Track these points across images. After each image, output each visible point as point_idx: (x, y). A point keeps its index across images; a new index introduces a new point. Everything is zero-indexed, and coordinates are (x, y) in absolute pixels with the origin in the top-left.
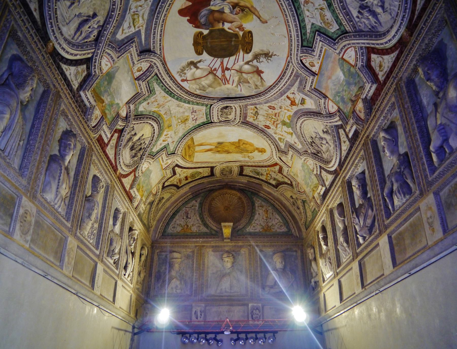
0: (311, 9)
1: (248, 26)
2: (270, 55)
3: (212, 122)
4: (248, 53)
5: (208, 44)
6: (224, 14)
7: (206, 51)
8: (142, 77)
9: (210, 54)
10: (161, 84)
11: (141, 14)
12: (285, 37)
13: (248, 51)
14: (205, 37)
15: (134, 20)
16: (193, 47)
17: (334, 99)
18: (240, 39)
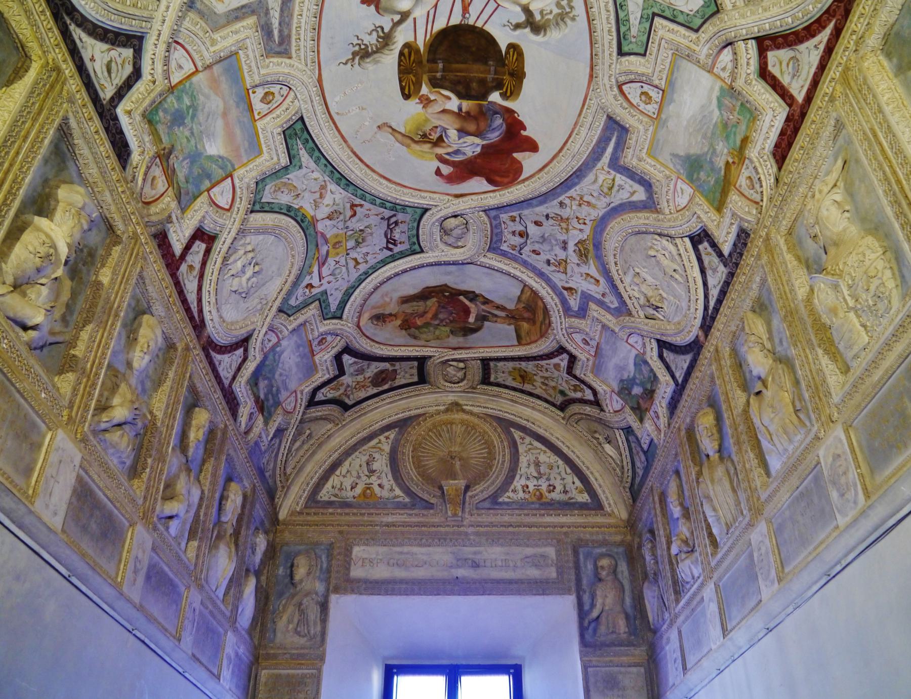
1: (413, 107)
2: (357, 58)
4: (407, 45)
5: (492, 69)
6: (457, 126)
7: (501, 51)
9: (490, 41)
10: (622, 15)
11: (596, 187)
12: (338, 114)
13: (406, 51)
14: (499, 86)
15: (610, 189)
16: (527, 69)
17: (191, 84)
18: (425, 78)
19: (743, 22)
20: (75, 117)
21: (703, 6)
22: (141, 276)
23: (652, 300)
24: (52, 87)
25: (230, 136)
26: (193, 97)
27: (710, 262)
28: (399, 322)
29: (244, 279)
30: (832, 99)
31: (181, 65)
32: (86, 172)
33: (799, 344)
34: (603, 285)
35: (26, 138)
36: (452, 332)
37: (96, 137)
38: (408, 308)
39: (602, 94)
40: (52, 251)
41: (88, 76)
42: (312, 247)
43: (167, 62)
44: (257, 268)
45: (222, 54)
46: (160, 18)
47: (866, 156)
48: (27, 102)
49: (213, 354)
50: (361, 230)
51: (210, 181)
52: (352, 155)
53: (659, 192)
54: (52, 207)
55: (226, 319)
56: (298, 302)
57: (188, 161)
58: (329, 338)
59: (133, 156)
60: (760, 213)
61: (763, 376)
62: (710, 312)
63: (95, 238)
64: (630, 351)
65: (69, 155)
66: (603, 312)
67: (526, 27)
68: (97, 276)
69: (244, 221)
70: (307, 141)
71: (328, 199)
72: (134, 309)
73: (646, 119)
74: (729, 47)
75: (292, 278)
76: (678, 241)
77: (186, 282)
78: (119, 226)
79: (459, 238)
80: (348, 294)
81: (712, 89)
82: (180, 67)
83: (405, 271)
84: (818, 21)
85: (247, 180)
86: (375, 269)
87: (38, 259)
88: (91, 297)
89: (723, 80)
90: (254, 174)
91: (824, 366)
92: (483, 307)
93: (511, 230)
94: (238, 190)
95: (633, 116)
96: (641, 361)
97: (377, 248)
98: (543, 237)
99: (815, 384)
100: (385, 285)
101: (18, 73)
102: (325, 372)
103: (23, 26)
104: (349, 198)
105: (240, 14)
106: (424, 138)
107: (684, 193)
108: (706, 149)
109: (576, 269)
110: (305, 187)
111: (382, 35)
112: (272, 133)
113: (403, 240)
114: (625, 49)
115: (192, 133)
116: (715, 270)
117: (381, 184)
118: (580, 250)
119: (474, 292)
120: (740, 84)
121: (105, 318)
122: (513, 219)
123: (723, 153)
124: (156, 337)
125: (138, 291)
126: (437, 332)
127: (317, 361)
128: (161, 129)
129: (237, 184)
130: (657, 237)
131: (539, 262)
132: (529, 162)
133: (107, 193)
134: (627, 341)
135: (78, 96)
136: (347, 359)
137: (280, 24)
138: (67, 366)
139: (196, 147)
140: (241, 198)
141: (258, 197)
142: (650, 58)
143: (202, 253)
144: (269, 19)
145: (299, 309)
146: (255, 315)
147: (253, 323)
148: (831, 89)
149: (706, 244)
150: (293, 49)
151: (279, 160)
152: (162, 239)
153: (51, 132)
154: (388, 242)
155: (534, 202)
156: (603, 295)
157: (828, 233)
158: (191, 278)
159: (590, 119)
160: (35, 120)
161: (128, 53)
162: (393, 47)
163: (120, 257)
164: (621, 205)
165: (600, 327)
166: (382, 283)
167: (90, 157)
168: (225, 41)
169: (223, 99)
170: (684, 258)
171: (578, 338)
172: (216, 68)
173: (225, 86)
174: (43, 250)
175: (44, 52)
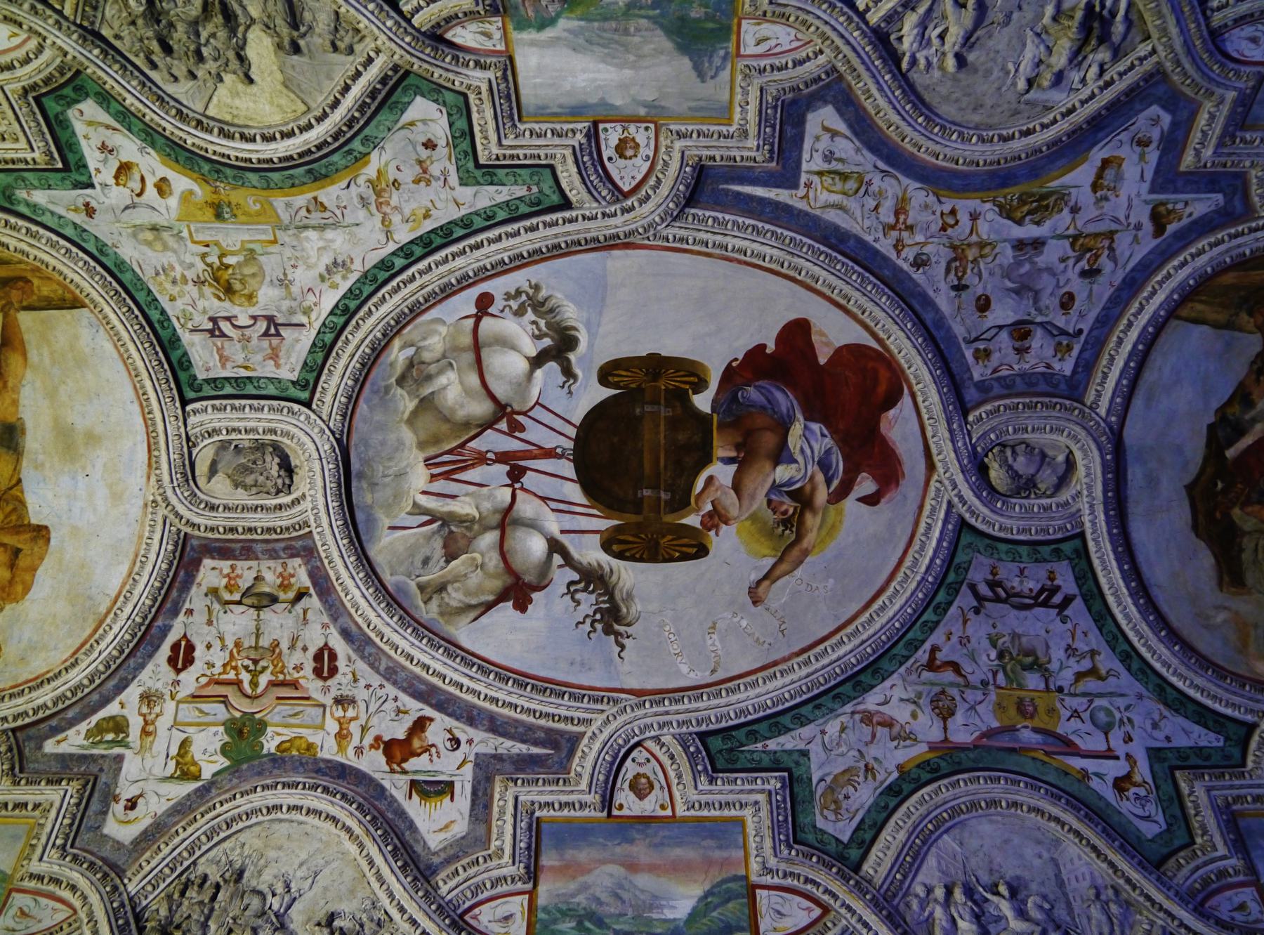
0: (851, 736)
1: (724, 542)
2: (616, 627)
3: (184, 402)
4: (606, 547)
5: (648, 408)
6: (768, 466)
7: (615, 396)
8: (591, 154)
9: (597, 414)
10: (502, 215)
11: (852, 204)
12: (713, 671)
13: (615, 547)
14: (680, 398)
15: (844, 177)
17: (545, 909)
18: (668, 518)
25: (678, 869)
42: (1011, 761)
50: (1001, 656)
56: (1160, 818)
67: (568, 361)
71: (901, 714)
80: (1179, 703)
81: (533, 43)
93: (1012, 357)
97: (1058, 626)
100: (1173, 619)
104: (909, 671)
105: (482, 801)
108: (643, 22)
109: (1089, 211)
111: (582, 585)
119: (1211, 428)
137: (524, 742)
144: (510, 757)
154: (1045, 604)
155: (928, 317)
156: (1143, 143)
162: (607, 569)
164: (873, 149)
169: (603, 862)
173: (583, 855)
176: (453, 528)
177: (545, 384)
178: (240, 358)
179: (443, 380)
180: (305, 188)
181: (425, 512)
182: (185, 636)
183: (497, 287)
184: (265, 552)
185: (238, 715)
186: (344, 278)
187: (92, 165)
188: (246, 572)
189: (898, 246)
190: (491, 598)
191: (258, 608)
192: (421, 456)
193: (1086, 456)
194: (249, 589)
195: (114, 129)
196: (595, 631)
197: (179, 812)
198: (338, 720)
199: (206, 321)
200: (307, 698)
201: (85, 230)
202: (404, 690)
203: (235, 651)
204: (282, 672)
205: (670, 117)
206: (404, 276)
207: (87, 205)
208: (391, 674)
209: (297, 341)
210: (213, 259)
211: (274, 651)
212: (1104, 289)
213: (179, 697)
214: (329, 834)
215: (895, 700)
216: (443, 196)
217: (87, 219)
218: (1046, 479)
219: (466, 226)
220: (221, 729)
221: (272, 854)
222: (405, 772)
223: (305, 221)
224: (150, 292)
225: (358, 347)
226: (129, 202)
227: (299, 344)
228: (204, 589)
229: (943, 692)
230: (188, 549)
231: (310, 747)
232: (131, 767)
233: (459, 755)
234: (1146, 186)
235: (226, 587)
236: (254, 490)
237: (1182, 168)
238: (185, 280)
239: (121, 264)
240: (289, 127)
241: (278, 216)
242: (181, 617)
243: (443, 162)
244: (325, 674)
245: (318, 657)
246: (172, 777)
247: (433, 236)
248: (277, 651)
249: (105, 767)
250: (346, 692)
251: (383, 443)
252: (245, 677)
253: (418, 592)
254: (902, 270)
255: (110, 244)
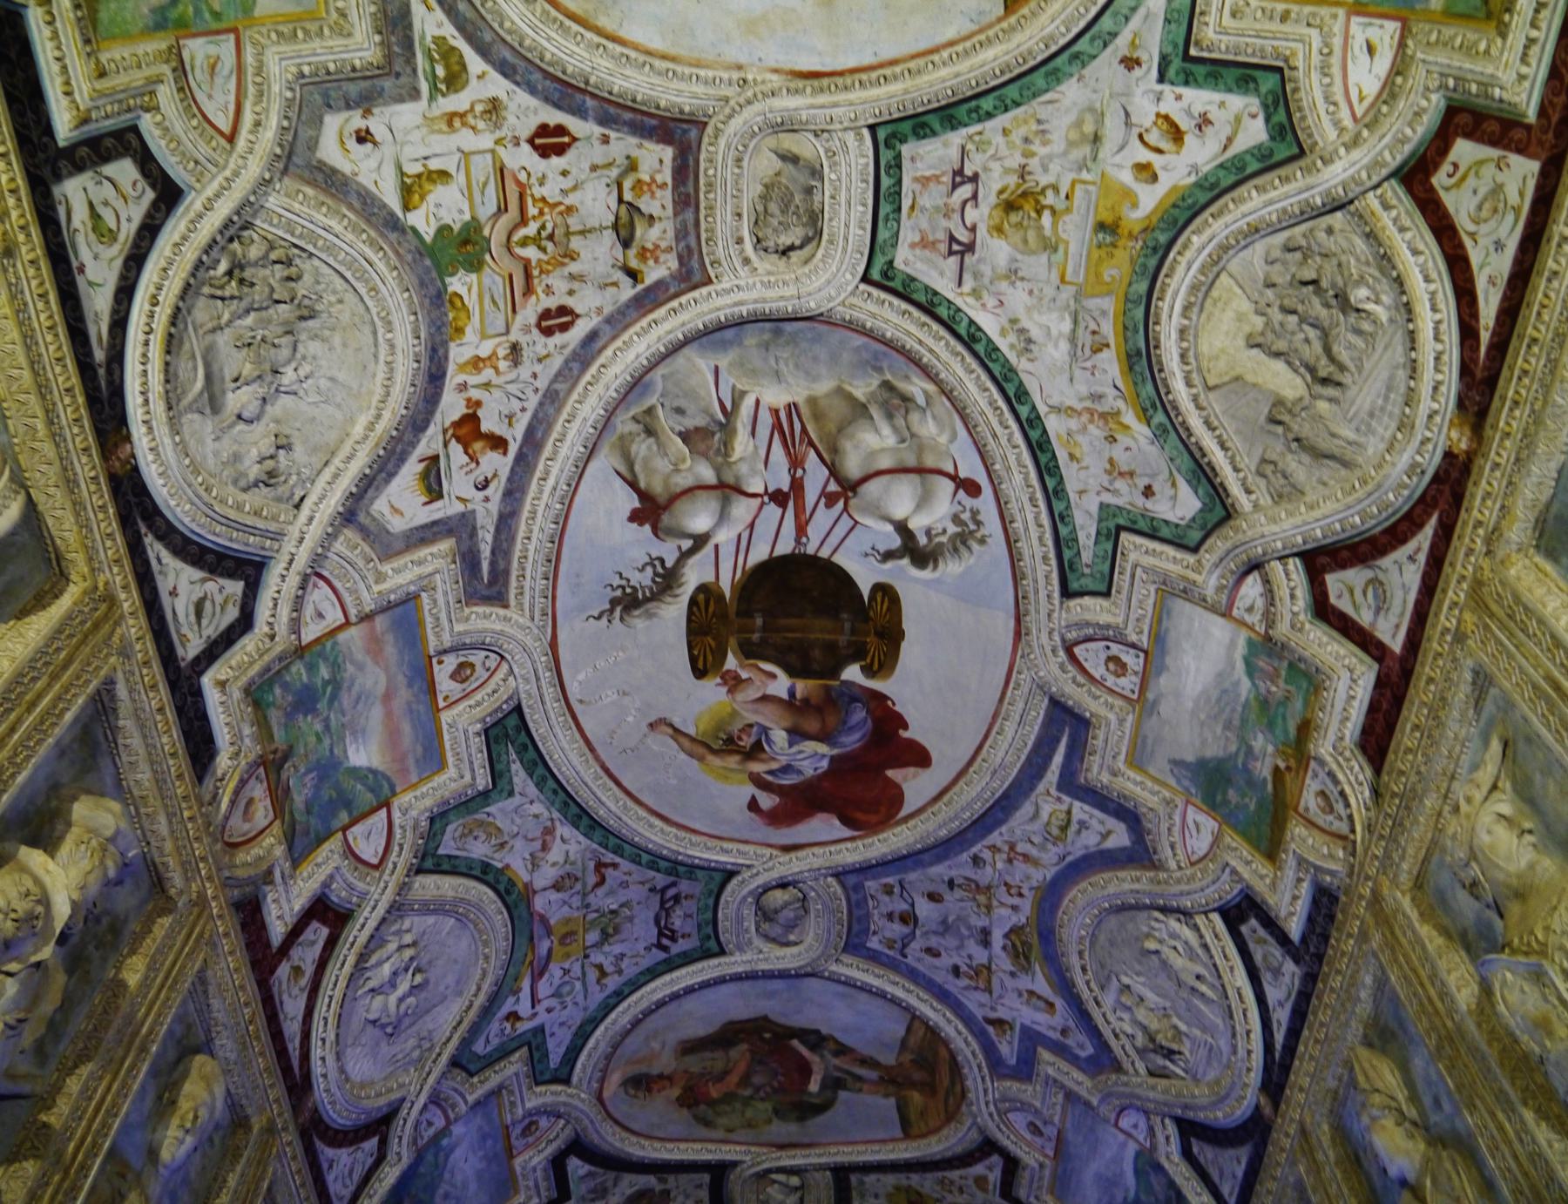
1: (711, 692)
2: (618, 610)
4: (702, 588)
5: (847, 626)
6: (787, 724)
7: (861, 596)
9: (843, 580)
10: (1063, 531)
11: (1037, 826)
12: (581, 701)
13: (701, 597)
14: (857, 654)
15: (1064, 828)
16: (906, 625)
17: (335, 644)
18: (733, 642)
19: (1275, 528)
20: (127, 681)
21: (1201, 511)
22: (201, 978)
23: (1160, 1038)
24: (97, 626)
25: (393, 735)
26: (336, 667)
27: (1265, 958)
28: (676, 1092)
29: (393, 999)
30: (1460, 637)
31: (323, 611)
32: (131, 777)
33: (1478, 1102)
34: (1062, 1014)
35: (33, 704)
36: (776, 1112)
37: (159, 718)
38: (694, 1063)
39: (1039, 661)
40: (40, 909)
41: (162, 619)
42: (522, 941)
43: (298, 604)
44: (419, 979)
45: (392, 597)
46: (297, 535)
47: (1548, 726)
48: (48, 646)
49: (319, 1144)
50: (613, 912)
51: (350, 814)
52: (602, 773)
53: (1155, 830)
54: (57, 834)
55: (353, 1077)
56: (489, 1049)
57: (314, 774)
58: (544, 1122)
59: (218, 759)
60: (1353, 854)
61: (1411, 1177)
62: (1277, 1055)
63: (125, 899)
64: (1123, 1146)
65: (104, 746)
66: (1064, 1066)
67: (901, 557)
68: (118, 969)
69: (403, 888)
70: (525, 747)
71: (556, 854)
72: (179, 1042)
73: (1119, 702)
74: (1256, 574)
75: (481, 999)
76: (1200, 920)
77: (285, 997)
78: (176, 879)
79: (791, 926)
81: (1232, 644)
82: (320, 615)
83: (690, 990)
84: (1408, 516)
85: (414, 813)
86: (635, 985)
87: (9, 924)
88: (100, 1009)
89: (1251, 628)
90: (428, 802)
91: (1544, 1144)
92: (836, 1061)
93: (884, 910)
94: (398, 832)
95: (1096, 698)
96: (1148, 1164)
97: (641, 946)
98: (944, 922)
99: (1533, 1187)
100: (653, 1017)
101: (41, 601)
102: (533, 1192)
103: (66, 526)
104: (595, 851)
105: (428, 534)
106: (730, 745)
107: (1201, 829)
109: (1010, 983)
110: (516, 829)
112: (466, 732)
113: (687, 930)
114: (1074, 585)
115: (327, 728)
116: (1277, 972)
117: (651, 826)
118: (1014, 945)
119: (817, 1032)
120: (1282, 630)
121: (120, 1052)
122: (888, 890)
123: (1266, 755)
124: (214, 1099)
125: (191, 1007)
126: (749, 1113)
127: (518, 1169)
128: (275, 716)
129: (397, 820)
130: (1157, 914)
131: (938, 970)
132: (916, 786)
133: (162, 819)
134: (1116, 1125)
135: (138, 647)
136: (576, 1167)
137: (493, 552)
138: (29, 1145)
139: (331, 751)
140: (401, 846)
141: (432, 845)
142: (1119, 598)
143: (321, 943)
144: (476, 544)
145: (490, 1061)
146: (407, 1071)
147: (401, 1086)
148: (1454, 621)
149: (1253, 922)
150: (512, 592)
151: (474, 778)
152: (250, 912)
153: (80, 701)
154: (660, 934)
155: (926, 857)
156: (1064, 1032)
157: (1501, 876)
158: (295, 991)
159: (1021, 705)
160: (54, 677)
161: (236, 587)
163: (167, 936)
165: (1060, 1097)
166: (648, 1013)
167: (142, 751)
168: (400, 575)
169: (387, 670)
170: (1214, 952)
171: (1019, 1120)
172: (380, 622)
173: (390, 650)
174: (22, 907)
175: (93, 570)
176: (717, 436)
177: (877, 533)
178: (925, 201)
179: (886, 430)
180: (1121, 339)
181: (736, 404)
182: (575, 139)
183: (986, 503)
184: (684, 223)
185: (486, 232)
186: (1012, 346)
187: (1189, 93)
188: (659, 204)
189: (994, 849)
190: (642, 485)
191: (616, 227)
192: (800, 400)
193: (793, 956)
194: (639, 210)
195: (1225, 148)
196: (613, 589)
197: (365, 203)
198: (494, 353)
199: (974, 168)
200: (514, 311)
201: (1105, 45)
202: (535, 416)
203: (562, 208)
204: (541, 272)
205: (1140, 716)
206: (1008, 415)
207: (1138, 63)
208: (552, 399)
209: (942, 274)
210: (1049, 199)
211: (565, 256)
212: (940, 977)
213: (501, 151)
214: (371, 393)
215: (566, 847)
216: (1091, 481)
217: (1120, 55)
218: (776, 930)
219: (1056, 492)
220: (467, 217)
221: (337, 340)
222: (446, 445)
223: (1082, 325)
224: (1017, 104)
225: (931, 351)
226: (1134, 119)
227: (938, 276)
228: (635, 153)
229: (577, 879)
230: (685, 126)
231: (460, 331)
232: (407, 115)
233: (470, 492)
234: (1028, 1023)
235: (639, 181)
236: (760, 208)
237: (1040, 1049)
238: (1028, 154)
239: (1056, 77)
240: (1192, 360)
241: (1093, 296)
242: (598, 130)
243: (1126, 496)
244: (544, 324)
245: (563, 310)
246: (403, 174)
247: (1049, 455)
248: (566, 260)
249: (403, 80)
250: (527, 353)
251: (815, 359)
252: (531, 229)
253: (645, 408)
254: (972, 845)
255: (1085, 72)
